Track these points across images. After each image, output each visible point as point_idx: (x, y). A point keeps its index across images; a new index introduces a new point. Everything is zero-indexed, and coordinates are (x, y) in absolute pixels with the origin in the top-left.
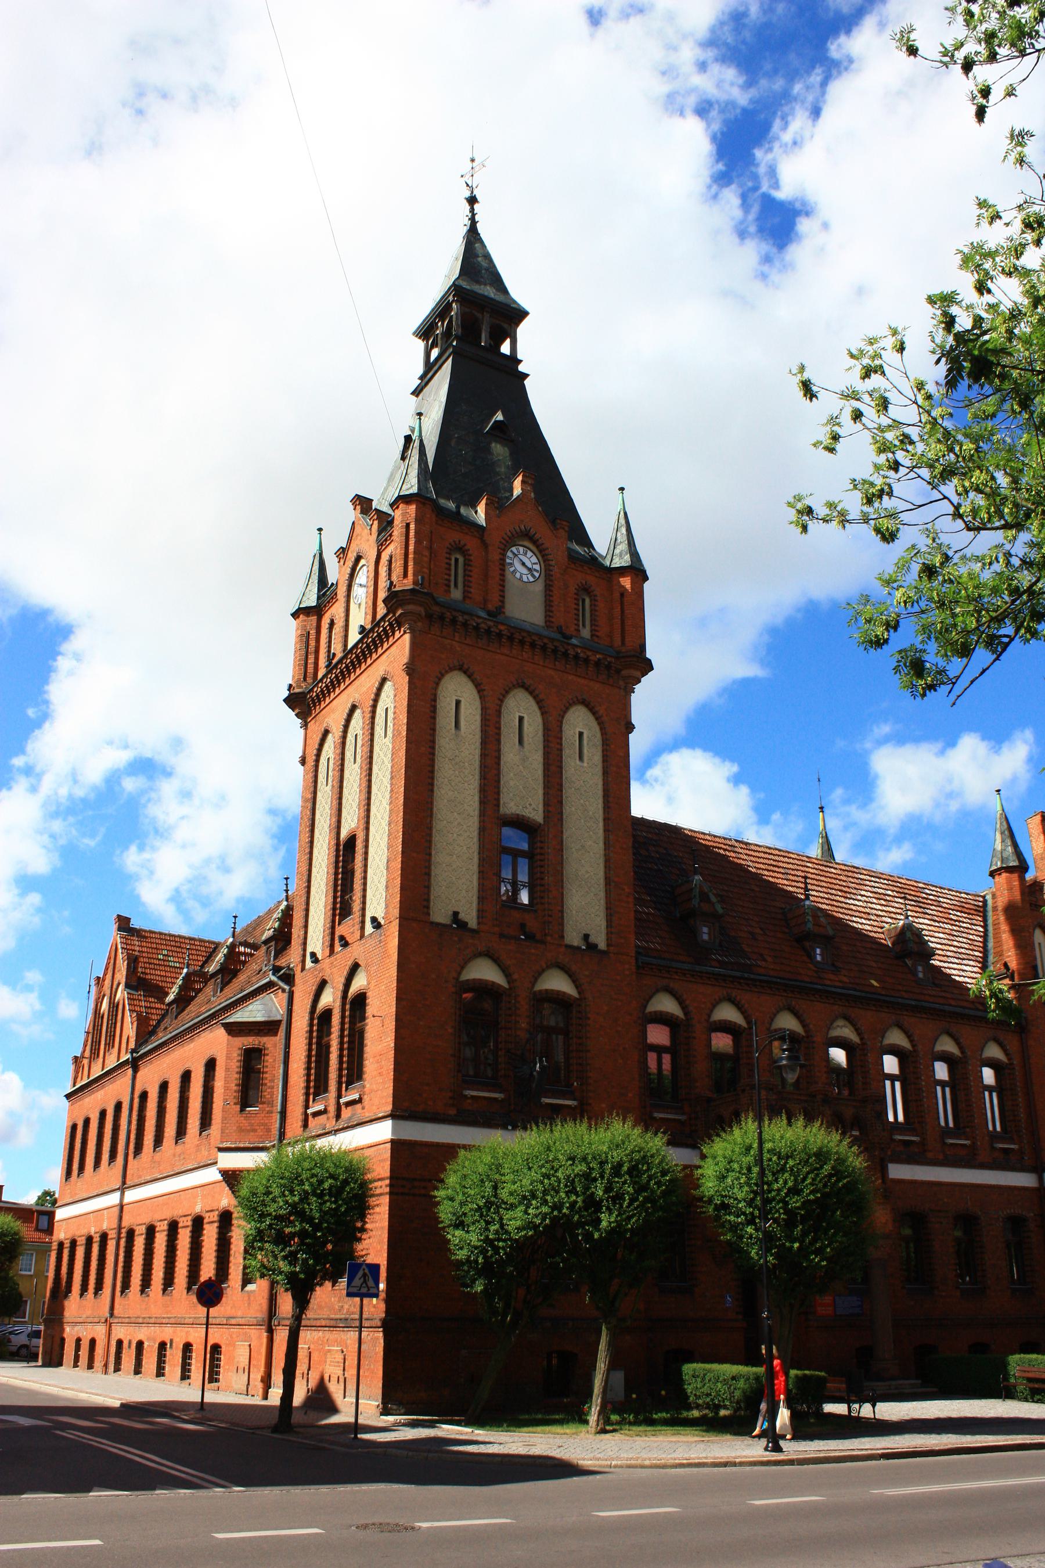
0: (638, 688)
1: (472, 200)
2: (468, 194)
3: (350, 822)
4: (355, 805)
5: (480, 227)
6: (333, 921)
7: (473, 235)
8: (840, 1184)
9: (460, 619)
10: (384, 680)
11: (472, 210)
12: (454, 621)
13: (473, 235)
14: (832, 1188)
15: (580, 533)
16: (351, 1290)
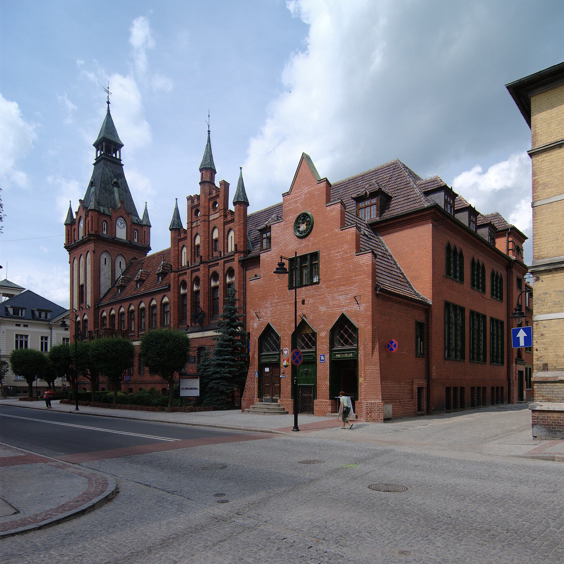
1: (108, 103)
2: (107, 101)
3: (82, 282)
4: (76, 293)
6: (79, 304)
11: (108, 106)
15: (138, 216)
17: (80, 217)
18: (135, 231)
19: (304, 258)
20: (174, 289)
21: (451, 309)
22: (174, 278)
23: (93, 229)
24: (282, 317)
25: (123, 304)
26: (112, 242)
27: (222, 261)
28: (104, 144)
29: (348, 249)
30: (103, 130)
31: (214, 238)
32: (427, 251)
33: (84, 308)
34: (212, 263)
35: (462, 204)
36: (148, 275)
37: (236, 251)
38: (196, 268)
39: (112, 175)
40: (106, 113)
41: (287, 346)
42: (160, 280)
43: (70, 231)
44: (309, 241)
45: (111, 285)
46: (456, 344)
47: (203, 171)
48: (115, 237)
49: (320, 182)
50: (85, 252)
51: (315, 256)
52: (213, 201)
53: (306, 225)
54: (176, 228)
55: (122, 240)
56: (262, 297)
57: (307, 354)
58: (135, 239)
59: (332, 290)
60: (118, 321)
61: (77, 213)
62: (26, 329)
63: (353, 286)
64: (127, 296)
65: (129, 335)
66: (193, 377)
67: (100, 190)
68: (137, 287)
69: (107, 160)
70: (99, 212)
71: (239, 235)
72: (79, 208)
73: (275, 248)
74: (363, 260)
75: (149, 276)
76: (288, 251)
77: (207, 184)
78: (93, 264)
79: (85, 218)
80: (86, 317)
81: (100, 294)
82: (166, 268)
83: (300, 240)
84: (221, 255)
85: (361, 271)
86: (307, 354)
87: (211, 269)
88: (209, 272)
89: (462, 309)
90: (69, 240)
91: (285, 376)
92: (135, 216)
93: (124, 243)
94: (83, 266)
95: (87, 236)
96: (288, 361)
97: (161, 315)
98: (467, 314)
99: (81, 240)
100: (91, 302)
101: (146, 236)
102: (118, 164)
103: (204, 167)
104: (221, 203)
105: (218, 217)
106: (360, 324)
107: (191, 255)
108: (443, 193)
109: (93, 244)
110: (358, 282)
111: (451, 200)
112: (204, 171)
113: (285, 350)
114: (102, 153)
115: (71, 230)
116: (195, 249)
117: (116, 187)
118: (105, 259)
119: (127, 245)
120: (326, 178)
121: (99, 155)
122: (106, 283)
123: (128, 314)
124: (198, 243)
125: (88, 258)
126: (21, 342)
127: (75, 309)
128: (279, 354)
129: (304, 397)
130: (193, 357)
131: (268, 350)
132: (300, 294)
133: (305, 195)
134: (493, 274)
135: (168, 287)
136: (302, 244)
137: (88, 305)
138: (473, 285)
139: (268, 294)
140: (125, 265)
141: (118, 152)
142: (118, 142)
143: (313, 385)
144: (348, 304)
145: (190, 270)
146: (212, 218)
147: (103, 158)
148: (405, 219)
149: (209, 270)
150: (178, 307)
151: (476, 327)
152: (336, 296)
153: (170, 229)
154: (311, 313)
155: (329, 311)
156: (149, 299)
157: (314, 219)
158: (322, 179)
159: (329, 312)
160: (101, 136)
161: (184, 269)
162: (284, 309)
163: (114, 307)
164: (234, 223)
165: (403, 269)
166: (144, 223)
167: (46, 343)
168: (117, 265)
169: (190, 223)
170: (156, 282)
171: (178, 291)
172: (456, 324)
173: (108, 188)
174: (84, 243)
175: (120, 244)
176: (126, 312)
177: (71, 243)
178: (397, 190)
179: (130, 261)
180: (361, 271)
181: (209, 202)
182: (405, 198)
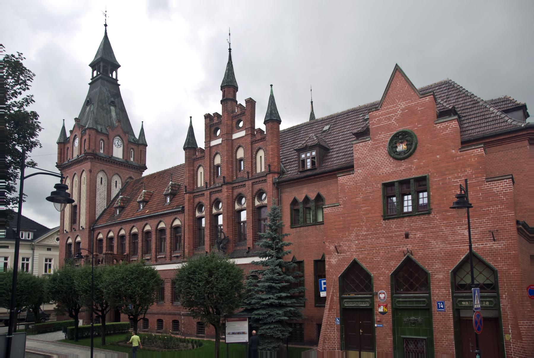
0: (119, 69)
1: (106, 25)
2: (105, 24)
6: (71, 225)
7: (106, 37)
9: (105, 159)
10: (83, 171)
11: (106, 28)
12: (103, 160)
13: (106, 37)
14: (191, 308)
15: (134, 136)
17: (76, 135)
18: (132, 150)
20: (188, 211)
22: (189, 200)
23: (90, 148)
24: (374, 253)
25: (123, 226)
26: (109, 161)
28: (102, 64)
29: (473, 174)
30: (100, 50)
32: (525, 175)
33: (77, 229)
34: (237, 185)
36: (151, 195)
37: (269, 171)
39: (109, 95)
41: (383, 288)
43: (63, 150)
44: (412, 163)
45: (107, 205)
47: (224, 88)
48: (112, 156)
50: (80, 171)
54: (192, 147)
55: (118, 159)
56: (342, 228)
57: (414, 299)
58: (131, 158)
59: (451, 222)
60: (118, 244)
61: (71, 132)
63: (485, 219)
64: (128, 218)
65: (131, 260)
66: (241, 319)
67: (97, 108)
68: (140, 208)
69: (104, 79)
70: (97, 131)
71: (272, 154)
72: (74, 127)
73: (360, 171)
74: (499, 187)
75: (153, 196)
76: (379, 174)
77: (229, 102)
78: (89, 183)
79: (80, 136)
80: (79, 239)
81: (95, 215)
82: (174, 189)
83: (396, 161)
84: (248, 176)
85: (495, 201)
86: (414, 299)
88: (232, 194)
90: (61, 158)
91: (382, 324)
92: (132, 135)
94: (77, 185)
95: (84, 155)
96: (386, 306)
97: (171, 239)
99: (76, 159)
100: (86, 224)
101: (142, 155)
102: (115, 84)
103: (227, 84)
106: (499, 265)
107: (210, 175)
109: (89, 163)
110: (492, 214)
112: (226, 88)
113: (381, 293)
115: (64, 148)
116: (214, 169)
117: (113, 106)
118: (102, 178)
119: (123, 164)
122: (101, 205)
123: (130, 237)
124: (217, 163)
127: (65, 230)
128: (372, 299)
132: (401, 226)
133: (403, 110)
135: (182, 210)
136: (401, 166)
137: (82, 227)
139: (352, 225)
142: (115, 63)
144: (478, 240)
147: (100, 78)
148: (493, 139)
149: (232, 192)
150: (193, 231)
152: (458, 230)
154: (420, 249)
155: (447, 247)
159: (447, 249)
160: (99, 57)
161: (201, 190)
162: (378, 244)
163: (113, 228)
164: (265, 142)
166: (141, 142)
167: (27, 264)
168: (113, 184)
171: (193, 214)
173: (105, 108)
174: (78, 161)
175: (117, 163)
176: (128, 234)
177: (64, 162)
179: (126, 180)
180: (495, 201)
181: (232, 120)
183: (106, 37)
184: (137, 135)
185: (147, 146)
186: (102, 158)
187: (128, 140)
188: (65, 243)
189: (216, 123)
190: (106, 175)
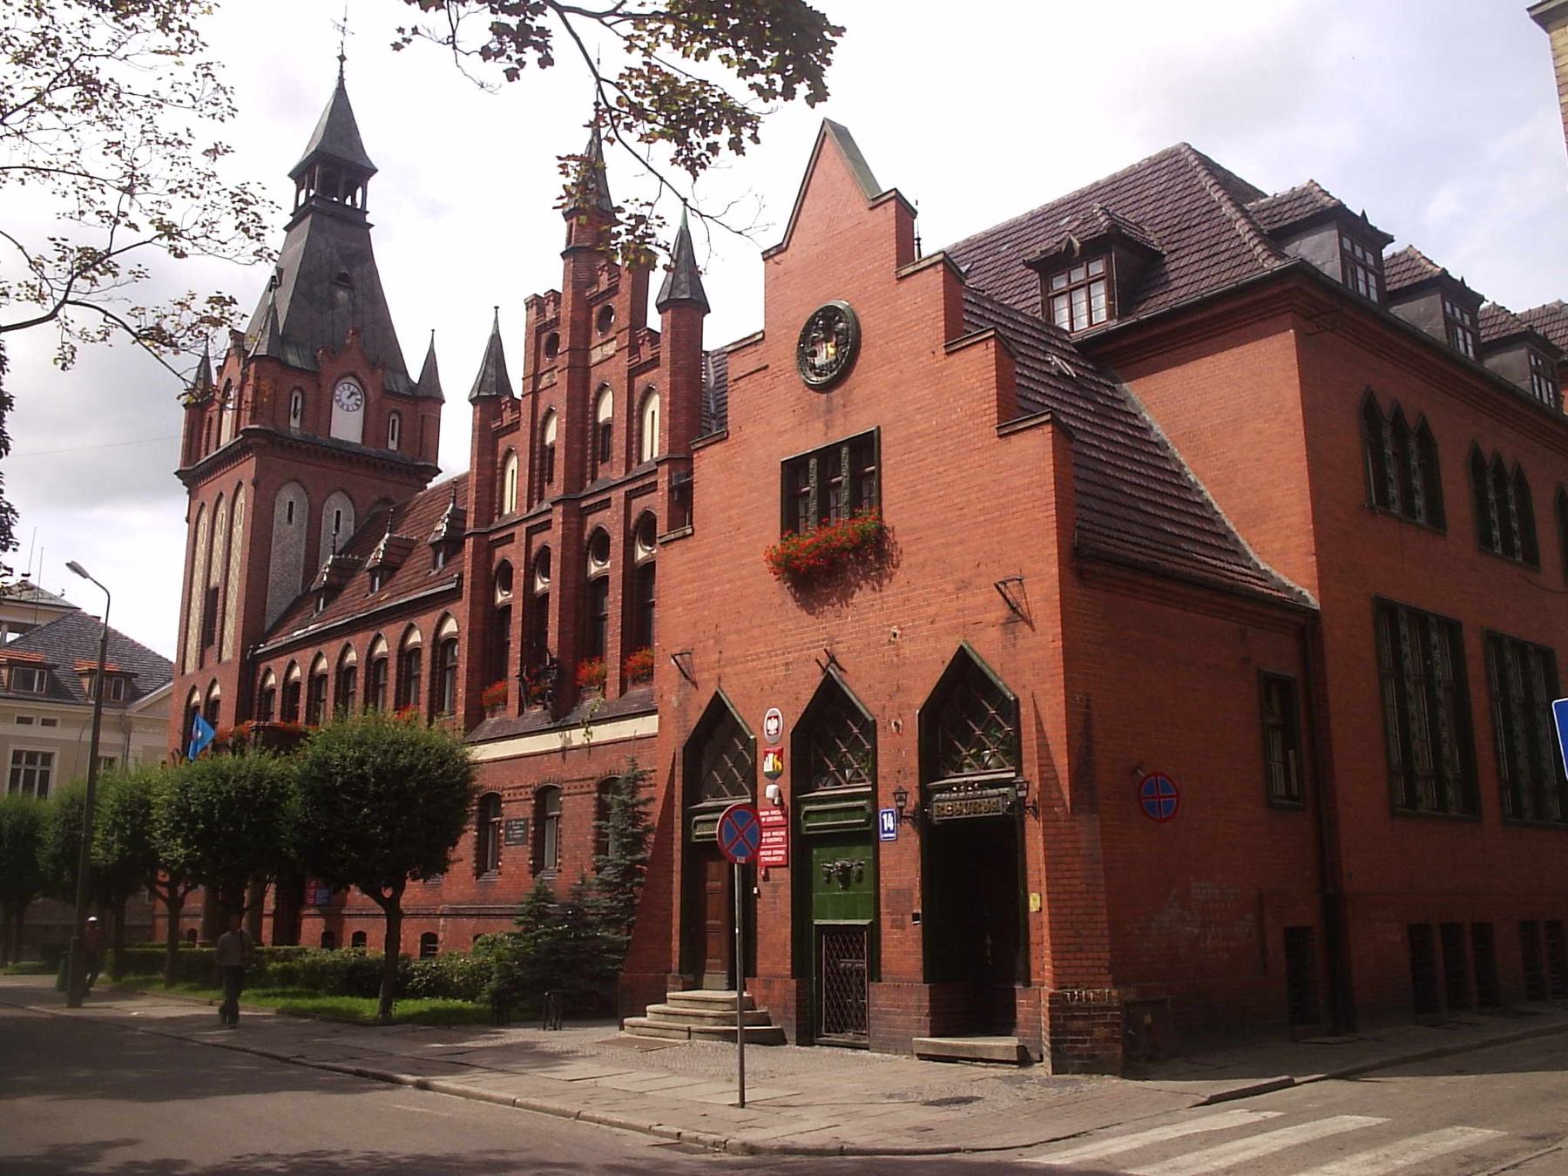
1: (342, 58)
5: (346, 83)
7: (341, 92)
8: (638, 866)
11: (341, 66)
12: (299, 448)
16: (854, 858)
19: (828, 456)
21: (1404, 629)
27: (622, 492)
31: (601, 419)
35: (1417, 272)
38: (542, 519)
39: (336, 257)
40: (334, 84)
42: (440, 565)
46: (1437, 753)
49: (878, 202)
51: (866, 447)
52: (599, 307)
53: (837, 345)
55: (348, 443)
61: (220, 369)
62: (48, 732)
69: (322, 213)
81: (264, 614)
87: (590, 518)
89: (1452, 628)
93: (355, 453)
98: (1473, 646)
102: (358, 223)
104: (623, 309)
105: (612, 352)
108: (1436, 299)
111: (1466, 316)
114: (312, 192)
118: (291, 503)
119: (285, 443)
120: (895, 189)
121: (302, 201)
125: (238, 504)
126: (30, 775)
129: (845, 974)
130: (520, 820)
131: (718, 794)
134: (1476, 462)
138: (1486, 542)
140: (353, 522)
141: (359, 192)
143: (866, 922)
145: (525, 525)
146: (596, 356)
151: (1517, 691)
153: (471, 401)
156: (400, 626)
157: (862, 324)
158: (884, 191)
165: (1210, 489)
169: (533, 376)
170: (427, 572)
172: (1429, 680)
174: (229, 457)
176: (333, 670)
178: (1179, 231)
182: (1205, 253)
183: (341, 92)
184: (415, 375)
185: (444, 402)
186: (304, 447)
187: (383, 385)
188: (184, 704)
189: (551, 321)
190: (307, 493)
